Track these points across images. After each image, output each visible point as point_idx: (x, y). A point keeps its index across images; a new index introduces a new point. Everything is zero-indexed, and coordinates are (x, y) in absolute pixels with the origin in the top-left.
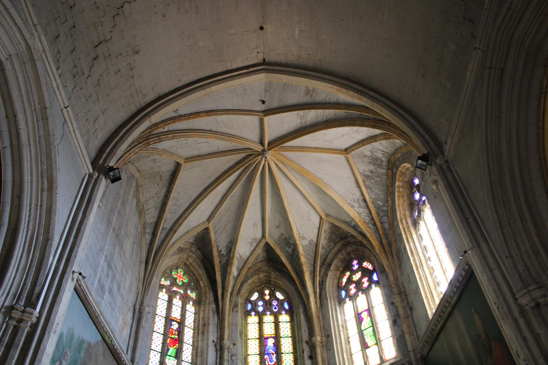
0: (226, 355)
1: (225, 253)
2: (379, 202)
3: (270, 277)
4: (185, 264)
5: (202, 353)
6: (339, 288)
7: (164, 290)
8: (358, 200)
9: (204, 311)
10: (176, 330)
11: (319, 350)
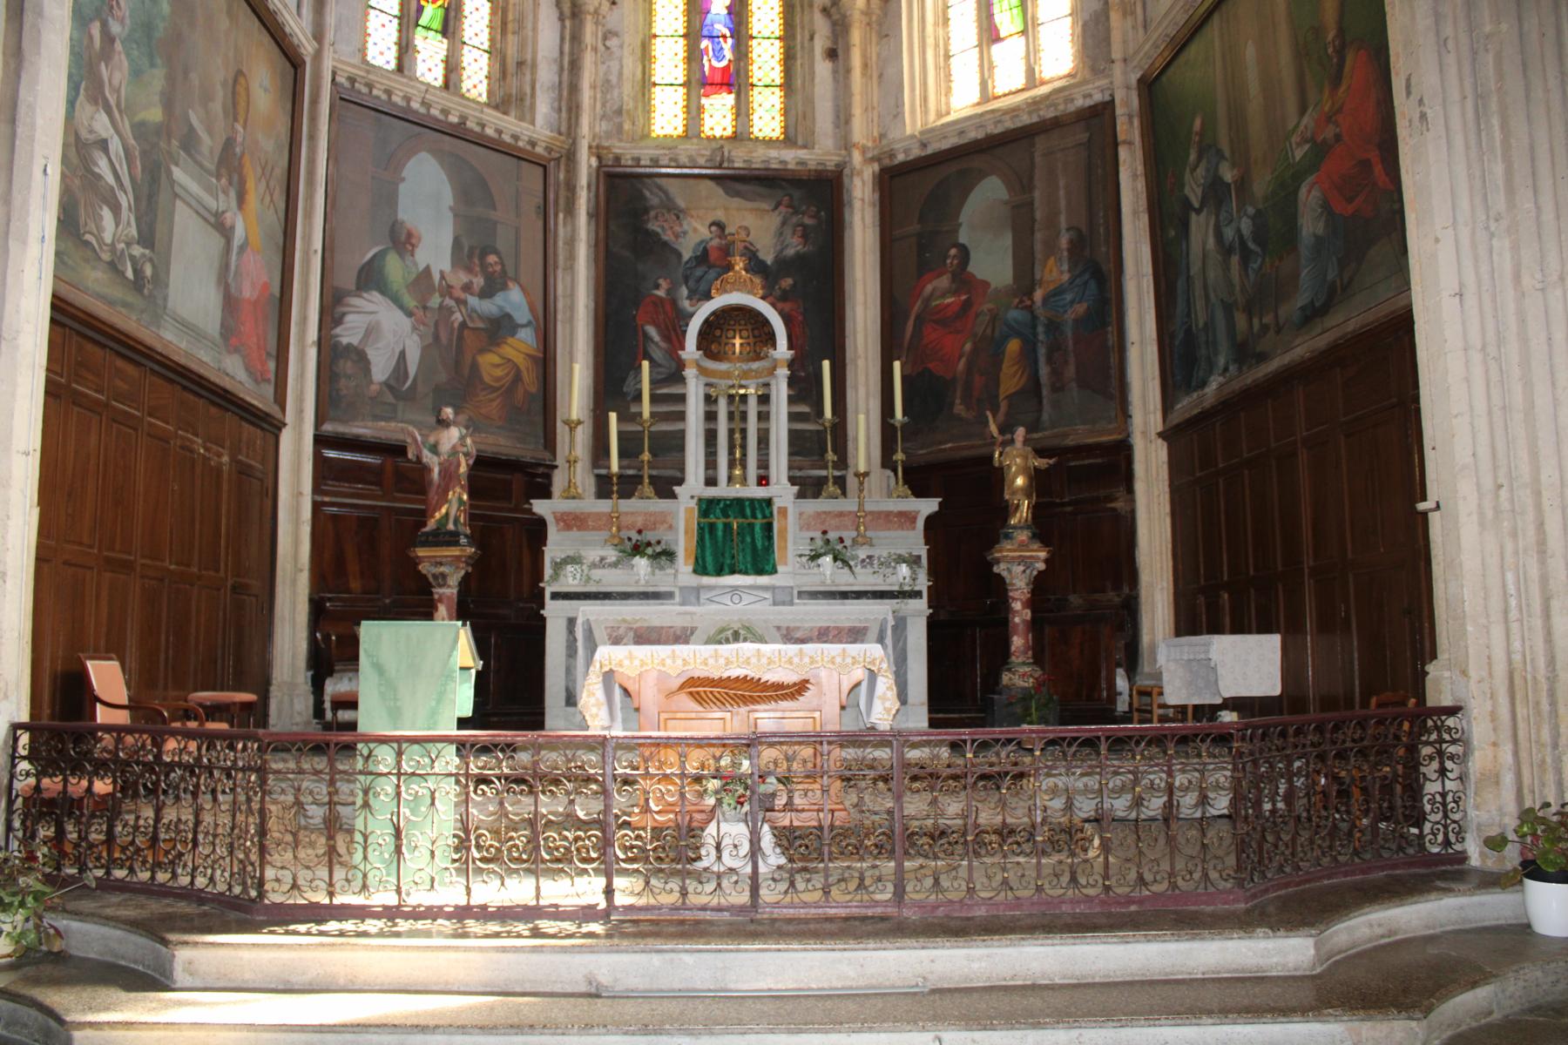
0: (590, 33)
5: (520, 22)
11: (856, 36)
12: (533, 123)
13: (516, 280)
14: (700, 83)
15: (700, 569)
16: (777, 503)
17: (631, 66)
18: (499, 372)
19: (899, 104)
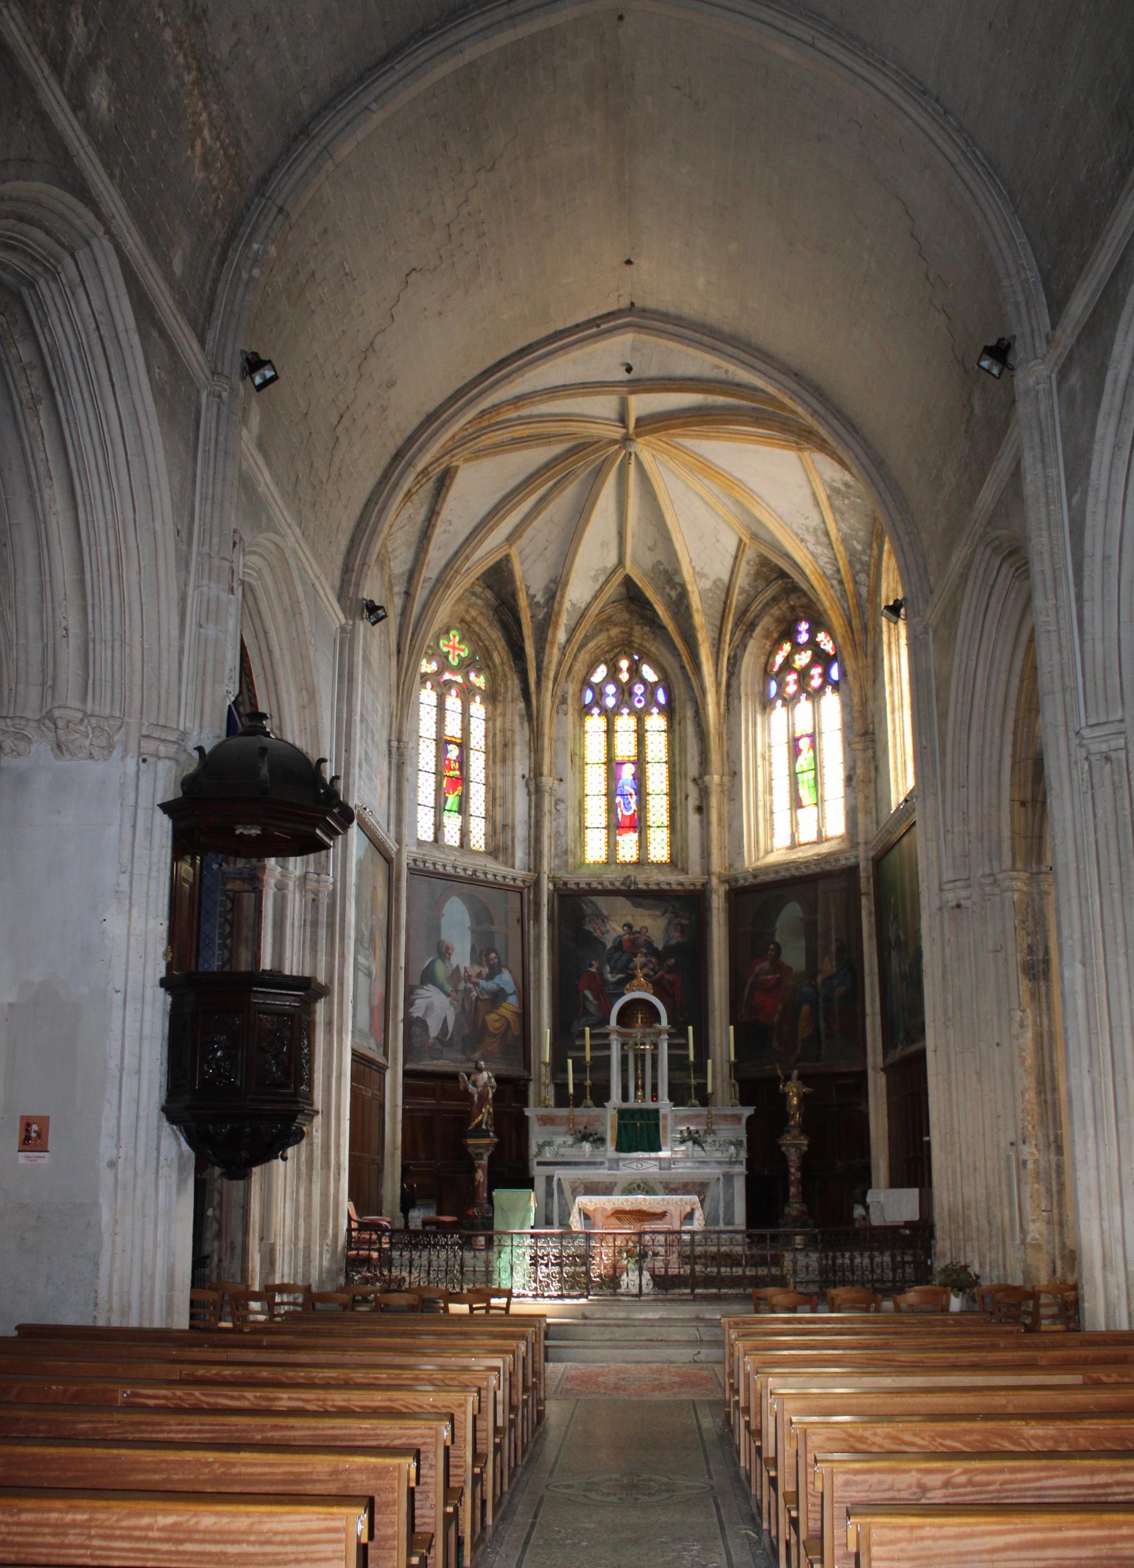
0: (547, 803)
1: (542, 601)
2: (855, 543)
3: (631, 635)
4: (462, 620)
5: (504, 798)
6: (767, 673)
7: (429, 684)
8: (815, 530)
9: (504, 715)
11: (714, 801)
12: (513, 867)
13: (506, 967)
14: (615, 827)
15: (619, 1148)
16: (662, 1112)
17: (572, 819)
18: (497, 1025)
19: (741, 846)
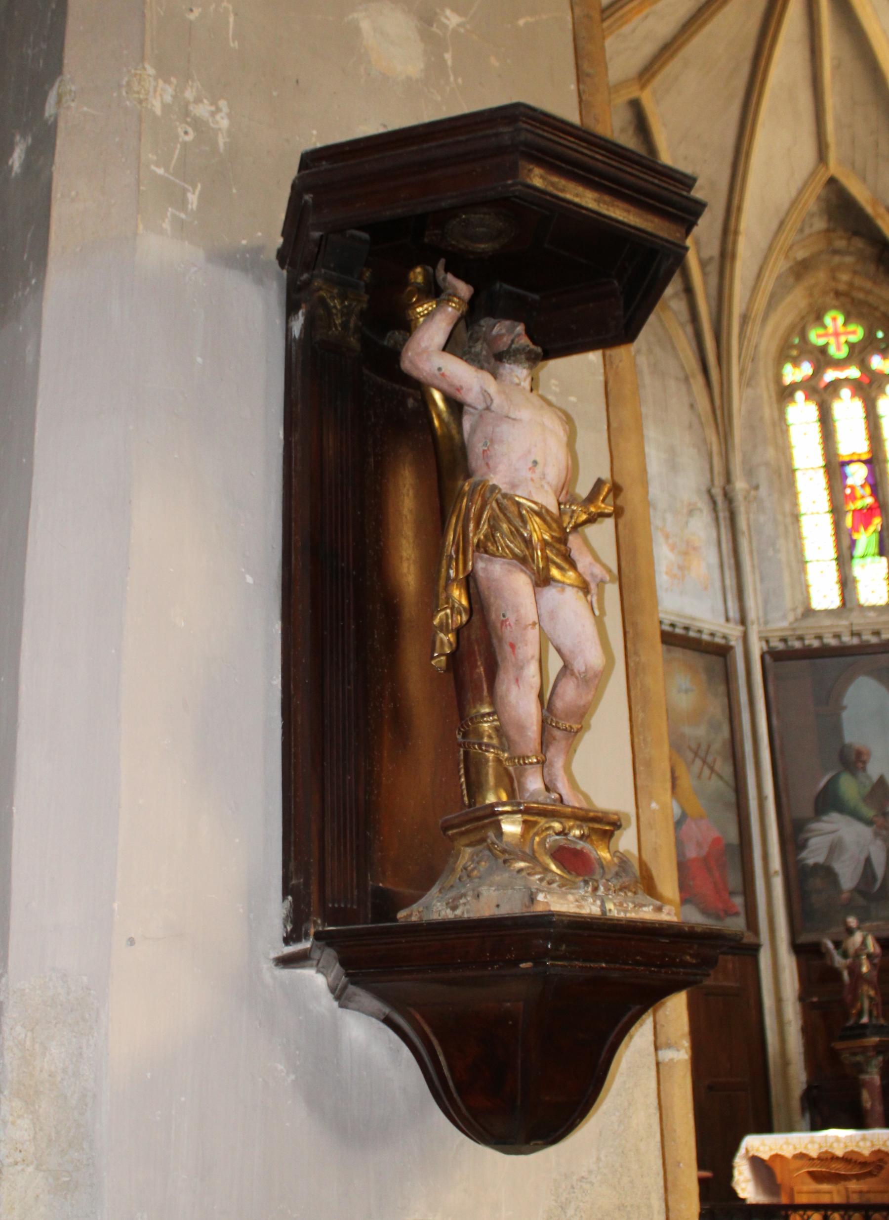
10: (862, 486)
